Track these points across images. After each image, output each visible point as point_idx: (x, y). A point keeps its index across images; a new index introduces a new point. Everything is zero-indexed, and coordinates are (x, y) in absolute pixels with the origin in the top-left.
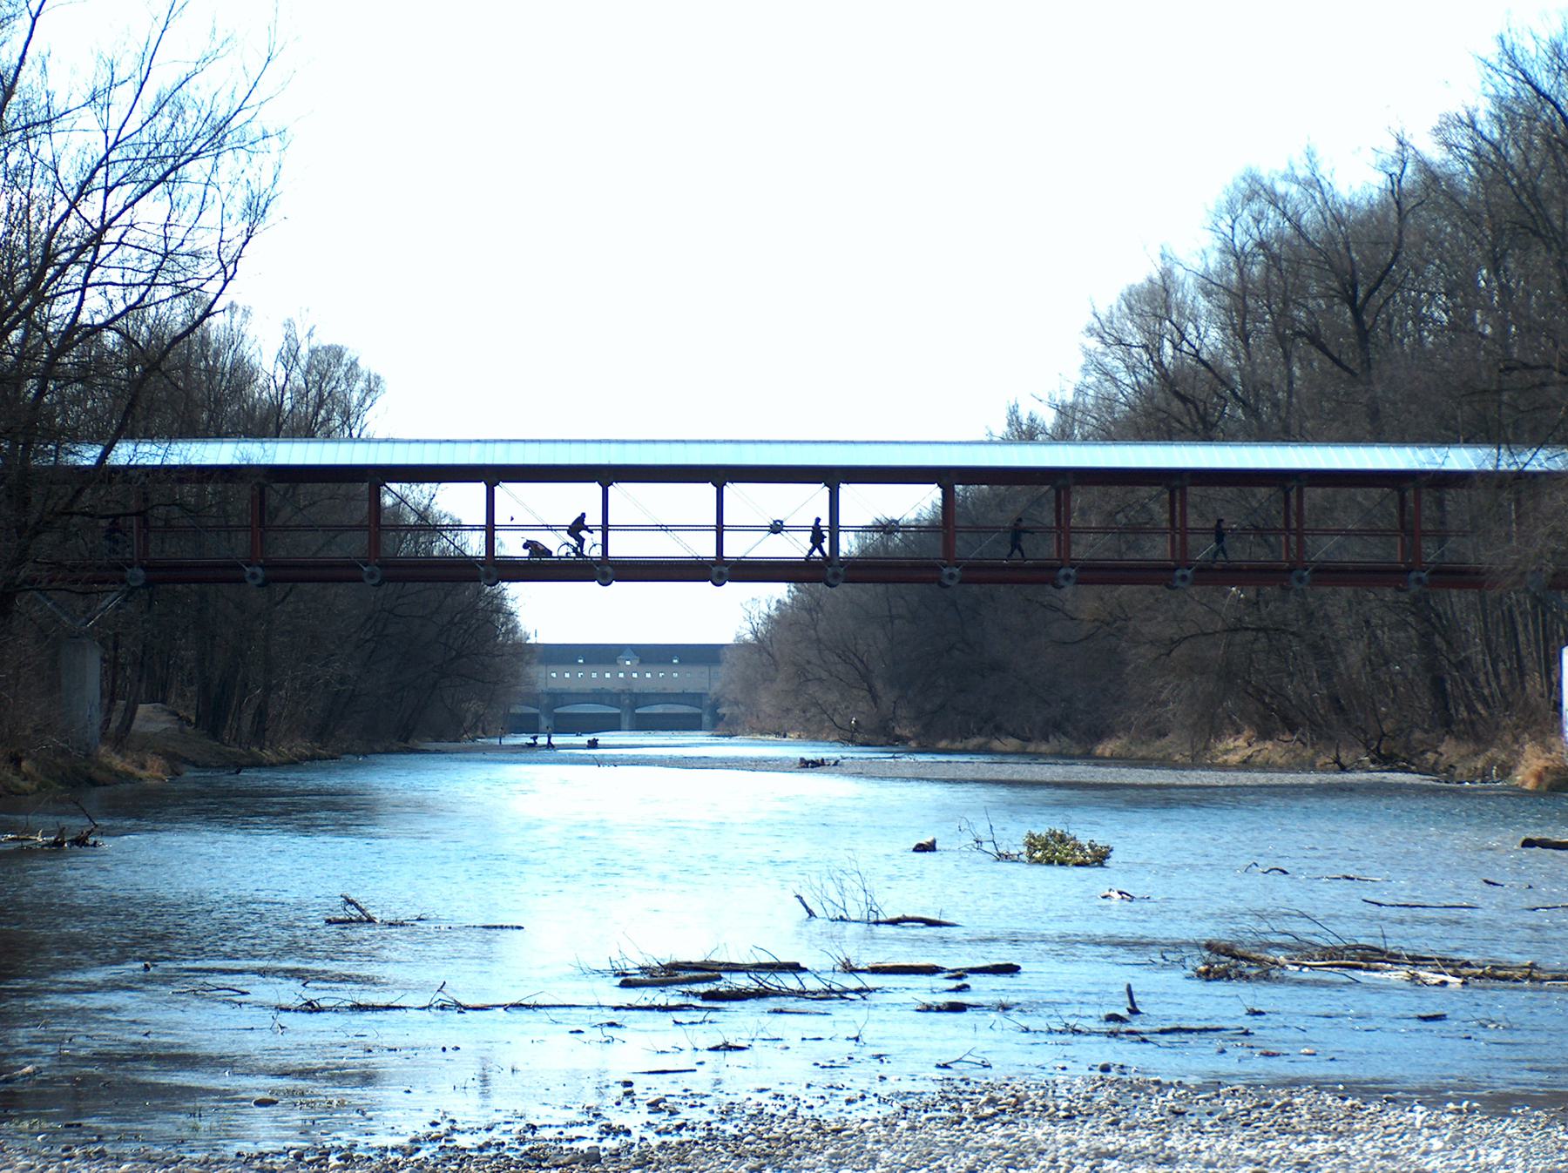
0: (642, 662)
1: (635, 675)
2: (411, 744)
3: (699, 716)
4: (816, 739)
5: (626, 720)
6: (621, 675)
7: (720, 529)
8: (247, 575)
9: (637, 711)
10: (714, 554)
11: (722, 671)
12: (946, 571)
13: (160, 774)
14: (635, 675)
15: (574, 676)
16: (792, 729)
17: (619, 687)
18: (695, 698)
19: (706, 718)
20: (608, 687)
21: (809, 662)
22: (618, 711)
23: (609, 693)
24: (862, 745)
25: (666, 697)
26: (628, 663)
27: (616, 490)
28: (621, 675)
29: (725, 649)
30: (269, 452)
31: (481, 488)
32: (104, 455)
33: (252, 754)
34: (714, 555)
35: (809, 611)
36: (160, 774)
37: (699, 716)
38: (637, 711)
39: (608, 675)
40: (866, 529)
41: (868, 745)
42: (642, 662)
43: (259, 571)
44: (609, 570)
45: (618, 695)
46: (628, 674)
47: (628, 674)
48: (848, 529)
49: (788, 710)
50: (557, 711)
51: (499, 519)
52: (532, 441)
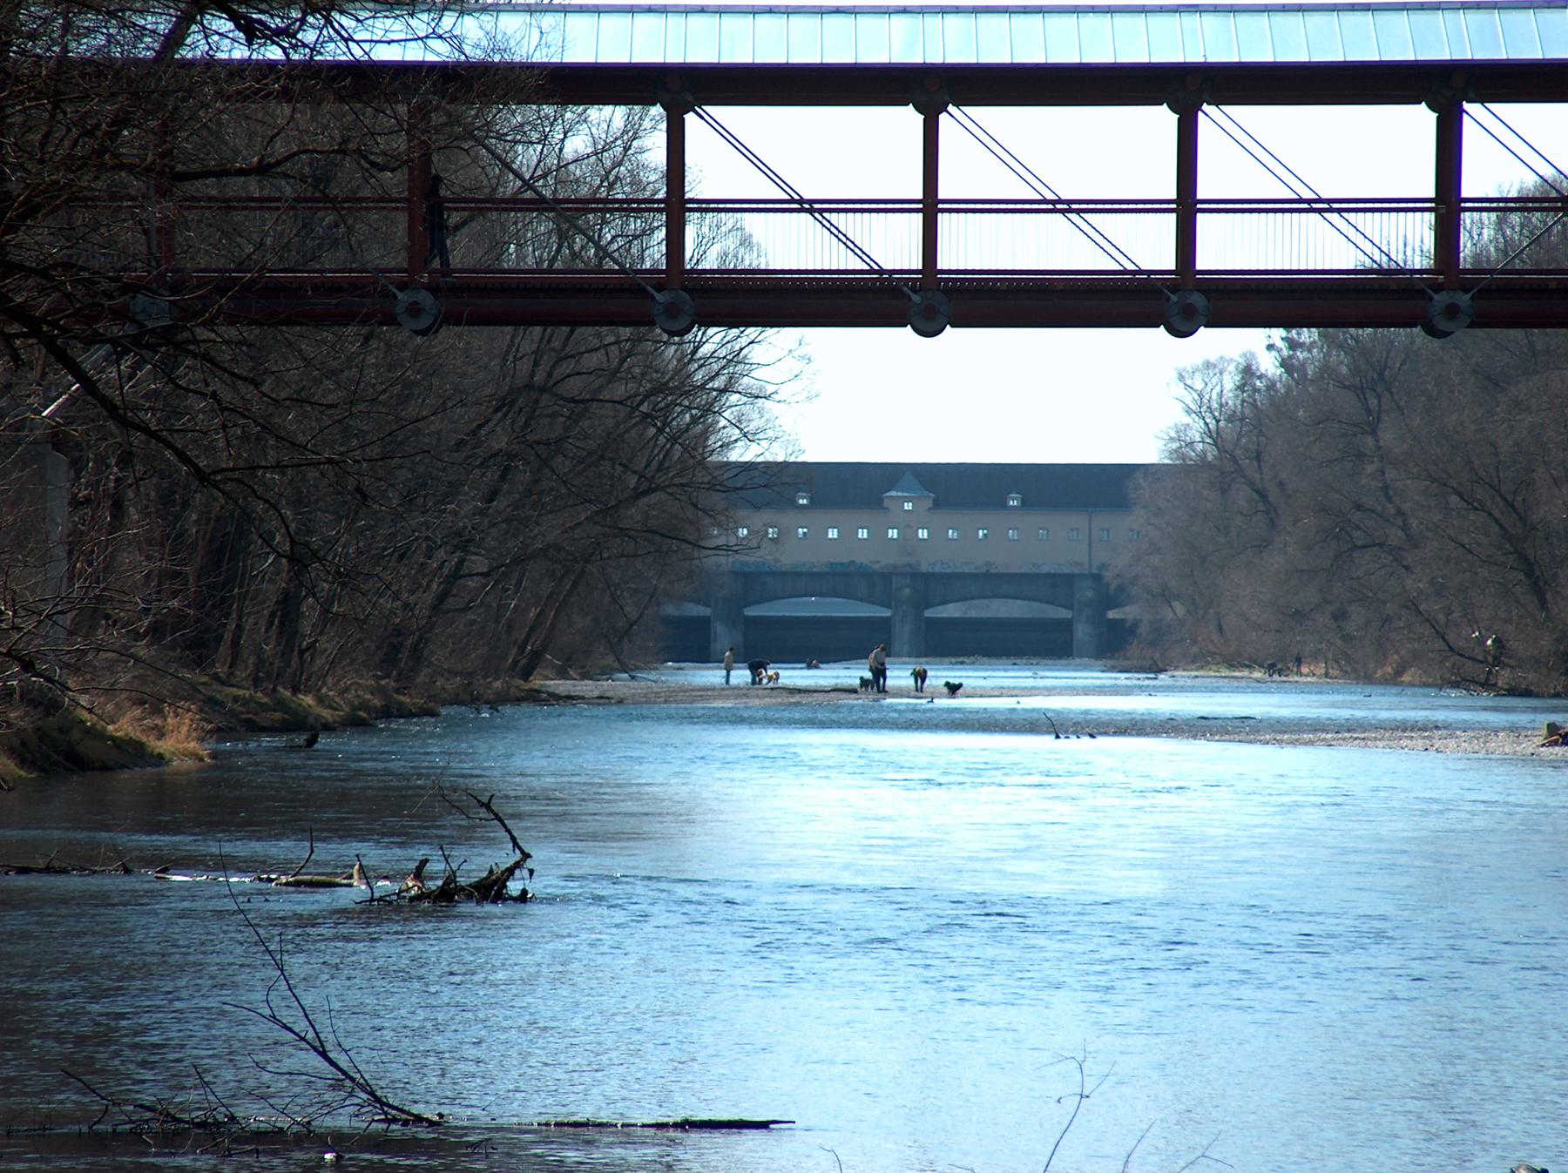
0: (937, 504)
1: (923, 534)
2: (537, 682)
3: (1066, 626)
4: (1369, 679)
5: (903, 633)
6: (893, 534)
7: (930, 206)
8: (400, 309)
9: (929, 613)
10: (916, 263)
11: (1136, 520)
12: (1441, 299)
13: (192, 745)
14: (923, 534)
15: (848, 535)
16: (1316, 657)
17: (887, 559)
18: (1057, 585)
19: (1082, 631)
20: (862, 558)
21: (1359, 507)
22: (887, 613)
23: (867, 574)
24: (1512, 692)
25: (992, 583)
26: (908, 506)
27: (1213, 121)
28: (893, 534)
29: (1139, 475)
30: (554, 38)
31: (1419, 120)
32: (175, 38)
33: (281, 705)
34: (1171, 265)
35: (1360, 391)
36: (192, 745)
37: (1066, 626)
38: (929, 613)
39: (863, 534)
40: (1523, 203)
41: (1528, 694)
42: (937, 504)
43: (425, 299)
44: (1198, 300)
45: (887, 576)
46: (908, 530)
47: (908, 530)
48: (1485, 204)
49: (1299, 615)
50: (751, 612)
51: (1206, 188)
52: (838, 11)
